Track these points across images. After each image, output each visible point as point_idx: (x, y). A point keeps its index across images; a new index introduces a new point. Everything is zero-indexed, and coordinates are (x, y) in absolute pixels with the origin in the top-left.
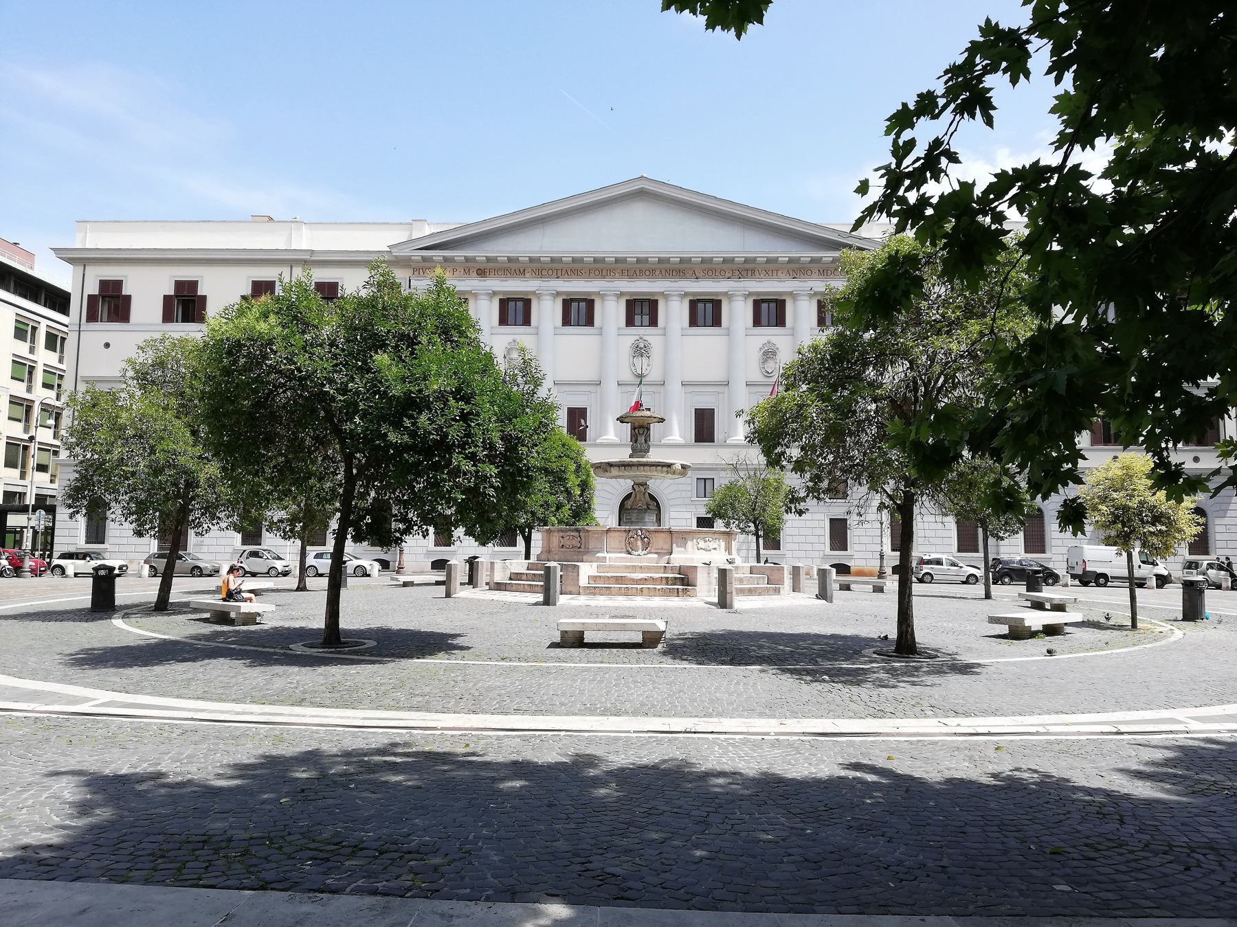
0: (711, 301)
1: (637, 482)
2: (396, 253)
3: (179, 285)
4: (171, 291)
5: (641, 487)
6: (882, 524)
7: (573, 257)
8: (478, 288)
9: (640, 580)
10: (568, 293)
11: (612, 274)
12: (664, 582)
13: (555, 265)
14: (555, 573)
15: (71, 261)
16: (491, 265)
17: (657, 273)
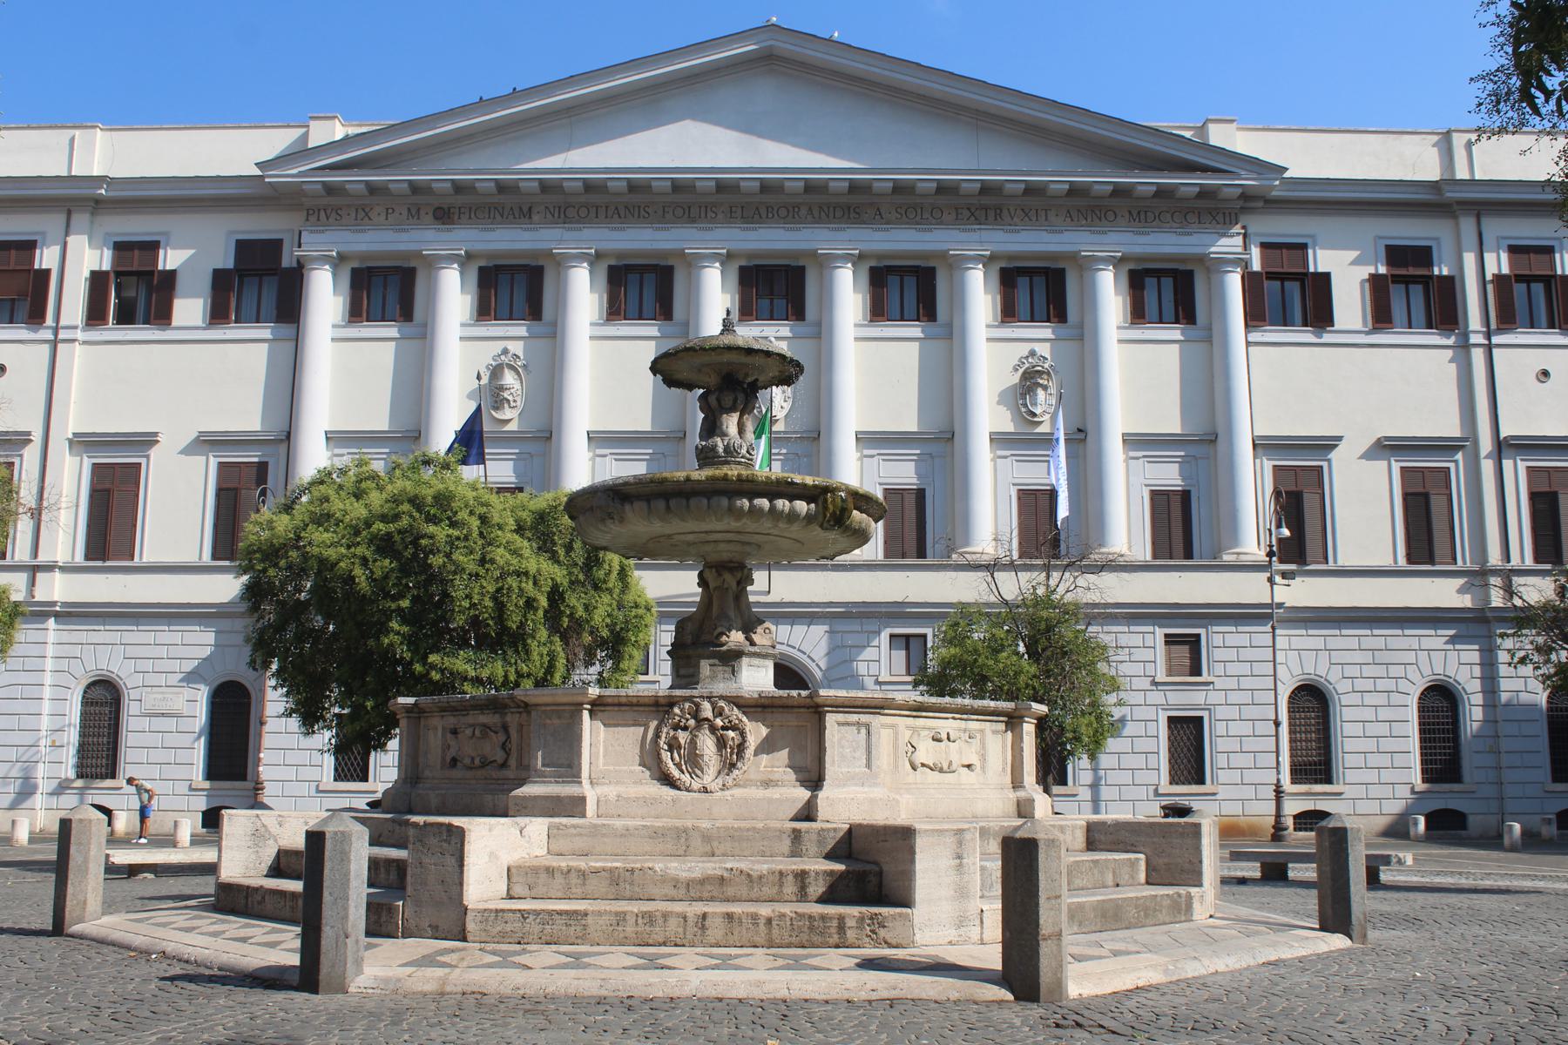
1: (713, 557)
3: (244, 248)
5: (727, 576)
6: (1277, 724)
9: (703, 881)
11: (710, 214)
12: (790, 888)
14: (344, 857)
16: (460, 200)
17: (804, 211)
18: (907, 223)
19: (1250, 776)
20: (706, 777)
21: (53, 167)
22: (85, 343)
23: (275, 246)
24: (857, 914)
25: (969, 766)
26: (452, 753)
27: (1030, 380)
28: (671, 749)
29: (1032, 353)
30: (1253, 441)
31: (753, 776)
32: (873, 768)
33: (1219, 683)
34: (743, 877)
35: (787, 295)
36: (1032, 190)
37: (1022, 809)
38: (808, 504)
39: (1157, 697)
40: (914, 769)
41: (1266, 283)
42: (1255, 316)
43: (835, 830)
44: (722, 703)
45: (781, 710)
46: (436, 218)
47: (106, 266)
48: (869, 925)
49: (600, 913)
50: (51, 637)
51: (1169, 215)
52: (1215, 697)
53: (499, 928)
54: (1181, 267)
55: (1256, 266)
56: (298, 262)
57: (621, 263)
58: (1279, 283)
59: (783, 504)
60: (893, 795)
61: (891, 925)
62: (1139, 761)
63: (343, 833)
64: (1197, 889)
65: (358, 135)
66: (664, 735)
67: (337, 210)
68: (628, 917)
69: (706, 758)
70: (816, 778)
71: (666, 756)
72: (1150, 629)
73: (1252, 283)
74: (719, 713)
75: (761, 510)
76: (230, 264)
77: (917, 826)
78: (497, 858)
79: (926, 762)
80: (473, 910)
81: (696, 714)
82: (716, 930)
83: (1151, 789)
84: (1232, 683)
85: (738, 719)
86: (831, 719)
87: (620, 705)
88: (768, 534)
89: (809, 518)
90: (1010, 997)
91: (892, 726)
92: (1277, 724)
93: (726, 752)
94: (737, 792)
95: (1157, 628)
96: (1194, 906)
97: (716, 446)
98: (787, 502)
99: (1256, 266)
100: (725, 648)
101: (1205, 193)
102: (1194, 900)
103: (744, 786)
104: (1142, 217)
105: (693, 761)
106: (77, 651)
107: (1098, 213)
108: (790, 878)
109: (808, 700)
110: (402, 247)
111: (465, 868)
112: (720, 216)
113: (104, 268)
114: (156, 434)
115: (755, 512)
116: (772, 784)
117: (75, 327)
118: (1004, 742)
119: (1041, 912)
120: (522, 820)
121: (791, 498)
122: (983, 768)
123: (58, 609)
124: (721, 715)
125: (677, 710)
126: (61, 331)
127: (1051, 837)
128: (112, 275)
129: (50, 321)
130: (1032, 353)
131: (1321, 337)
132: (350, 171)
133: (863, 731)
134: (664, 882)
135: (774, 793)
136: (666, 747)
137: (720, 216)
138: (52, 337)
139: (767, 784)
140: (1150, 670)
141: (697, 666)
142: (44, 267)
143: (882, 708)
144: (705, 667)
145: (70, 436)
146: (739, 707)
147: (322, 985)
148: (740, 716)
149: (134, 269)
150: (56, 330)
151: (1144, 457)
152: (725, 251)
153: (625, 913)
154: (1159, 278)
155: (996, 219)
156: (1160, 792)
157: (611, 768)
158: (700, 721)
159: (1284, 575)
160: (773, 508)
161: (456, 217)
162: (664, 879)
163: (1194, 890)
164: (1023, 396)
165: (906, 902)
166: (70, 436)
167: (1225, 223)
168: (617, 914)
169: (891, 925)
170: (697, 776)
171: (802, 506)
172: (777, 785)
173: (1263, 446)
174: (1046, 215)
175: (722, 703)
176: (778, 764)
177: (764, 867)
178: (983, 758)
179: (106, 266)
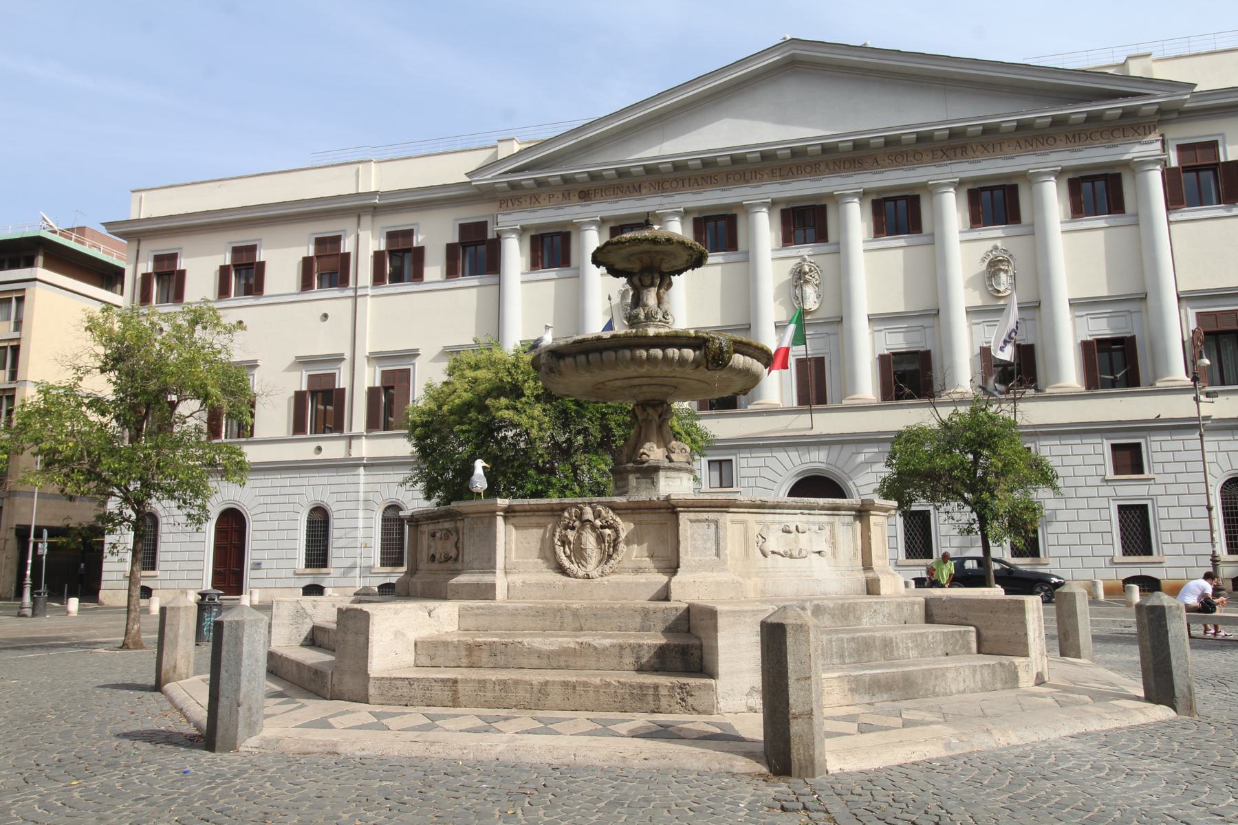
0: (1104, 177)
2: (481, 180)
3: (464, 229)
4: (454, 238)
7: (1018, 121)
8: (582, 216)
10: (879, 191)
11: (758, 176)
13: (738, 167)
15: (123, 235)
16: (595, 184)
18: (896, 166)
19: (1191, 549)
20: (589, 566)
21: (348, 189)
22: (373, 296)
23: (482, 226)
24: (669, 684)
25: (819, 553)
26: (432, 552)
27: (994, 266)
28: (563, 544)
29: (996, 248)
30: (1178, 295)
31: (626, 564)
32: (722, 556)
33: (1159, 479)
34: (591, 650)
35: (815, 225)
36: (988, 130)
37: (870, 588)
38: (694, 351)
39: (1108, 491)
40: (765, 556)
41: (1183, 176)
42: (1174, 200)
43: (677, 609)
44: (600, 508)
45: (646, 511)
46: (580, 198)
47: (383, 248)
48: (679, 694)
49: (466, 681)
50: (362, 479)
51: (1099, 134)
52: (1155, 490)
53: (392, 693)
54: (1111, 172)
55: (1174, 162)
56: (498, 235)
57: (701, 216)
58: (1195, 174)
59: (673, 352)
60: (741, 580)
61: (697, 694)
62: (1097, 539)
63: (237, 622)
64: (1022, 660)
65: (526, 149)
66: (557, 534)
67: (518, 199)
68: (488, 685)
69: (589, 551)
70: (675, 566)
71: (559, 550)
72: (1100, 441)
73: (1170, 177)
74: (598, 515)
75: (656, 358)
76: (456, 240)
77: (719, 608)
78: (403, 635)
79: (776, 550)
80: (374, 678)
81: (580, 517)
82: (556, 694)
83: (1108, 559)
84: (1171, 478)
85: (613, 519)
86: (684, 518)
87: (525, 511)
88: (674, 377)
89: (696, 363)
90: (764, 770)
91: (743, 522)
92: (1209, 509)
93: (605, 546)
94: (613, 578)
95: (1104, 440)
96: (1019, 674)
97: (638, 314)
98: (676, 350)
99: (1174, 162)
100: (646, 465)
101: (1127, 114)
102: (1019, 670)
103: (619, 573)
104: (1077, 138)
105: (579, 554)
106: (377, 487)
107: (1041, 140)
108: (628, 650)
109: (665, 503)
110: (560, 219)
111: (370, 644)
112: (766, 176)
113: (382, 249)
114: (417, 350)
115: (651, 360)
116: (641, 571)
117: (367, 287)
118: (854, 531)
119: (791, 691)
120: (431, 604)
121: (680, 347)
122: (834, 554)
123: (365, 462)
124: (599, 516)
125: (566, 514)
126: (358, 290)
127: (799, 622)
128: (387, 253)
129: (351, 284)
130: (996, 248)
131: (1231, 211)
132: (524, 173)
133: (713, 526)
134: (530, 653)
135: (641, 578)
136: (559, 543)
137: (766, 176)
138: (353, 294)
139: (638, 570)
140: (1101, 470)
141: (626, 479)
142: (346, 251)
143: (728, 507)
144: (632, 480)
145: (368, 354)
146: (613, 509)
147: (218, 744)
148: (614, 517)
149: (399, 248)
150: (356, 289)
151: (1087, 314)
152: (770, 200)
153: (485, 681)
154: (1093, 182)
155: (962, 155)
156: (1115, 561)
157: (521, 560)
158: (584, 522)
159: (1208, 395)
160: (665, 356)
161: (593, 196)
162: (531, 651)
163: (1018, 661)
164: (990, 278)
165: (712, 675)
166: (368, 354)
167: (1145, 134)
168: (479, 682)
169: (697, 694)
170: (583, 565)
171: (689, 353)
172: (644, 572)
173: (1184, 298)
174: (1001, 147)
175: (600, 508)
176: (632, 554)
177: (607, 642)
178: (834, 546)
179: (383, 248)
